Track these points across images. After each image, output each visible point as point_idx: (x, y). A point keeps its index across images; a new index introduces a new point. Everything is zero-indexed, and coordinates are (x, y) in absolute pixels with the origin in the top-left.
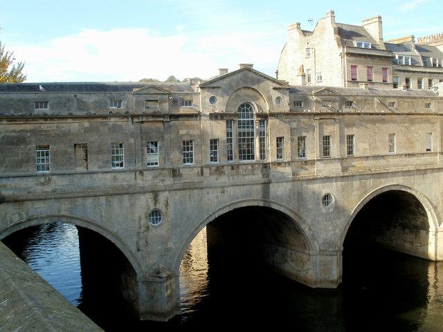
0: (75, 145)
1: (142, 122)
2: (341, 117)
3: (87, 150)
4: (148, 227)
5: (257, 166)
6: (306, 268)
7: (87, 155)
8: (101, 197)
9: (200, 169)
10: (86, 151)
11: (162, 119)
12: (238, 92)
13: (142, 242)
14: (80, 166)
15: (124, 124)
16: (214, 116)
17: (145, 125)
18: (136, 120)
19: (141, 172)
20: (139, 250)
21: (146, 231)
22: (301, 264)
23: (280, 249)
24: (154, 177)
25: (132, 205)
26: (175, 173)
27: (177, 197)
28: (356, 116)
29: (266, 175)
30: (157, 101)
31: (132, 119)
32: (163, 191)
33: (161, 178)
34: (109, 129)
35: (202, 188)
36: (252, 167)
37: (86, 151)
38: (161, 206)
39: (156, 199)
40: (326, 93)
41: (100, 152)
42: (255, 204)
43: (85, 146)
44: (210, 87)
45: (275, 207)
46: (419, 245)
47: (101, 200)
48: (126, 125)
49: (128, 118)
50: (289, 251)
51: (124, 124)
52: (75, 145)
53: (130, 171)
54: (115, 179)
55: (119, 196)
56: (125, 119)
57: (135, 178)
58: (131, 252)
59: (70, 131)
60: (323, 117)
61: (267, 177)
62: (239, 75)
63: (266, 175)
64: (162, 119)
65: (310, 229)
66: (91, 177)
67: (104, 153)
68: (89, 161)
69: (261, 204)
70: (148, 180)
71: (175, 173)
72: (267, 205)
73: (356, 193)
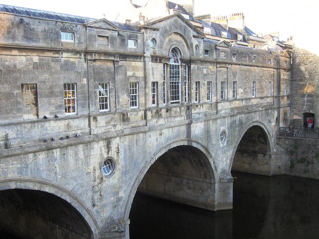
0: (22, 85)
1: (95, 60)
2: (230, 66)
3: (36, 91)
4: (102, 178)
5: (183, 108)
6: (206, 194)
7: (36, 99)
8: (54, 151)
9: (143, 112)
10: (36, 94)
11: (113, 58)
12: (170, 37)
13: (97, 196)
14: (28, 112)
15: (76, 61)
16: (155, 59)
17: (98, 64)
18: (89, 57)
19: (95, 118)
20: (94, 206)
21: (100, 183)
22: (201, 191)
23: (173, 179)
24: (106, 123)
25: (87, 157)
26: (125, 118)
27: (126, 143)
28: (237, 66)
29: (189, 116)
30: (108, 37)
31: (85, 55)
32: (115, 137)
33: (113, 123)
34: (61, 66)
35: (145, 132)
36: (180, 109)
37: (36, 94)
38: (113, 154)
39: (108, 147)
40: (223, 45)
41: (51, 94)
42: (182, 144)
43: (35, 89)
44: (151, 29)
45: (194, 145)
46: (257, 165)
47: (55, 154)
48: (79, 62)
49: (81, 55)
50: (185, 181)
51: (76, 61)
52: (22, 85)
53: (83, 116)
54: (69, 126)
55: (74, 147)
56: (78, 56)
57: (89, 125)
58: (87, 210)
59: (15, 66)
60: (221, 65)
61: (189, 118)
62: (172, 20)
63: (189, 116)
64: (113, 58)
65: (214, 163)
66: (42, 126)
67: (57, 96)
68: (39, 105)
69: (186, 144)
70: (101, 126)
71: (125, 118)
72: (190, 144)
73: (237, 128)
